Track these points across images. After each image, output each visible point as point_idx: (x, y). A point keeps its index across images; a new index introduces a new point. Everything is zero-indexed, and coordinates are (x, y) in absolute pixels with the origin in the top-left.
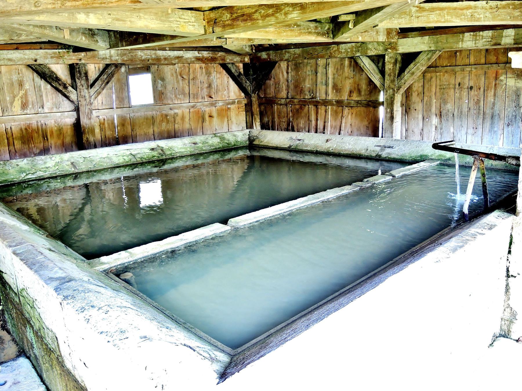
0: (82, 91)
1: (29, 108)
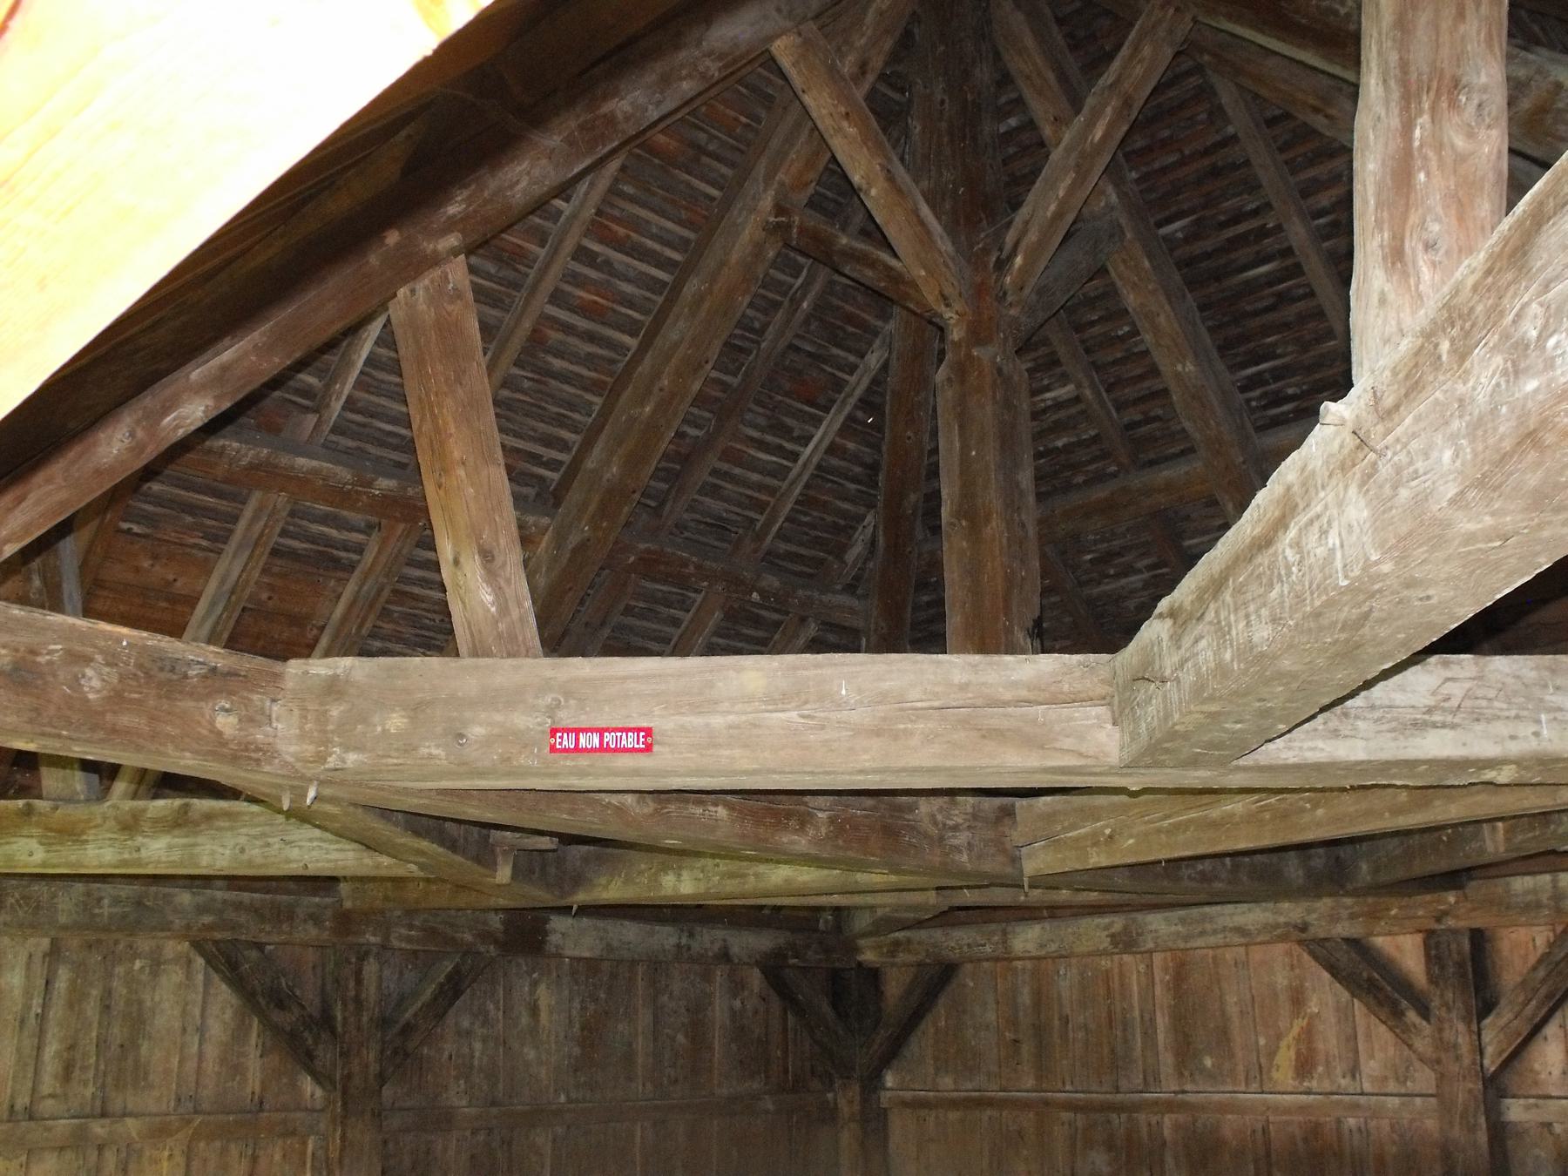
0: (1446, 1026)
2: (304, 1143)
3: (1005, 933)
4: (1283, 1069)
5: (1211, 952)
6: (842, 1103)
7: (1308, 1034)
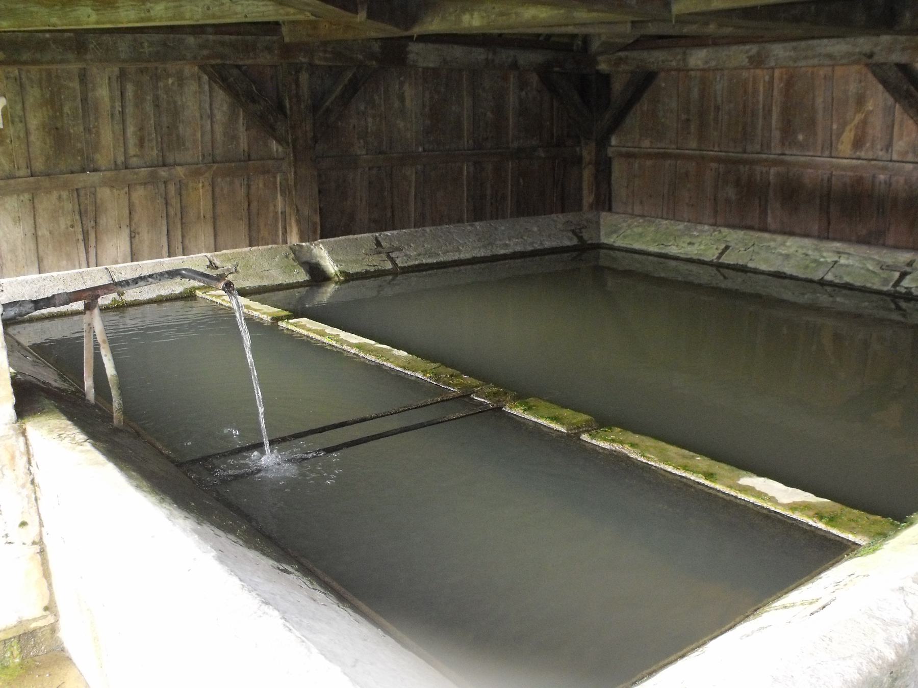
1: (864, 149)
2: (275, 177)
3: (684, 53)
4: (845, 145)
5: (810, 70)
6: (585, 153)
7: (864, 122)
